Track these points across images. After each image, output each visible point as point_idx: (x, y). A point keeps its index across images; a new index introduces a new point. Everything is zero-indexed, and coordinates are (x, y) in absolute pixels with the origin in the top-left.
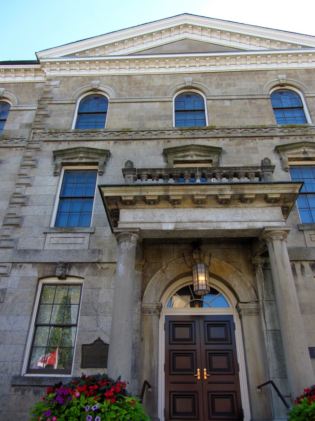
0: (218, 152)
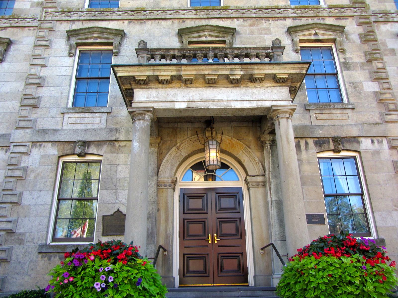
0: (232, 33)
